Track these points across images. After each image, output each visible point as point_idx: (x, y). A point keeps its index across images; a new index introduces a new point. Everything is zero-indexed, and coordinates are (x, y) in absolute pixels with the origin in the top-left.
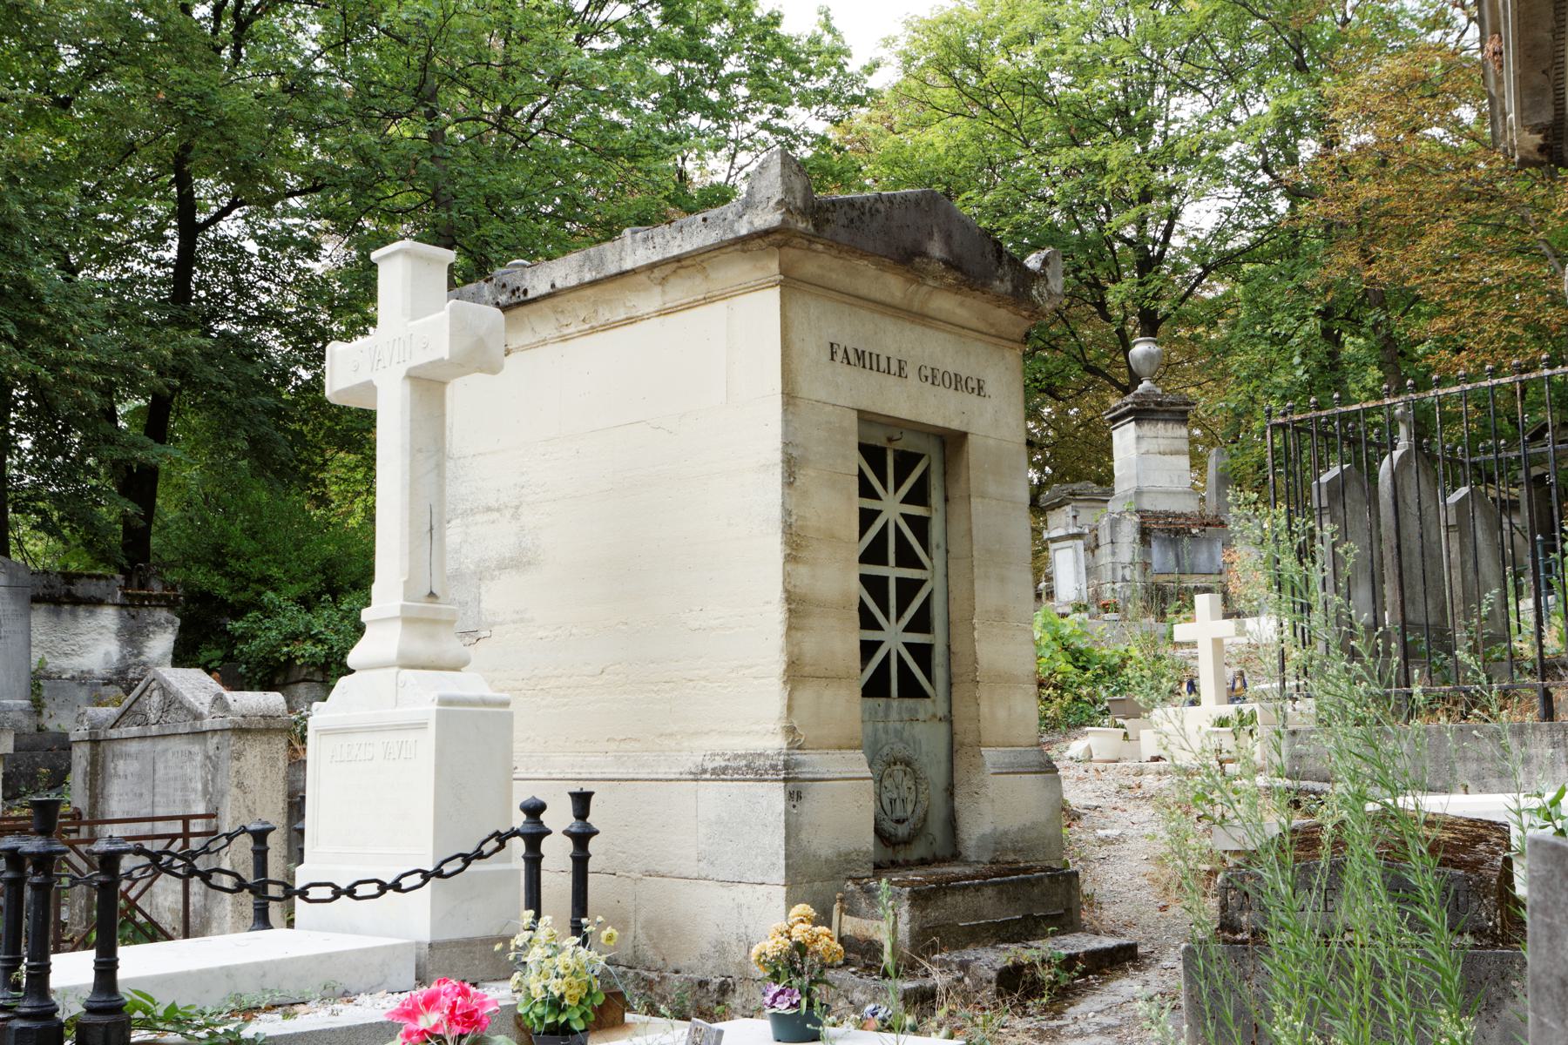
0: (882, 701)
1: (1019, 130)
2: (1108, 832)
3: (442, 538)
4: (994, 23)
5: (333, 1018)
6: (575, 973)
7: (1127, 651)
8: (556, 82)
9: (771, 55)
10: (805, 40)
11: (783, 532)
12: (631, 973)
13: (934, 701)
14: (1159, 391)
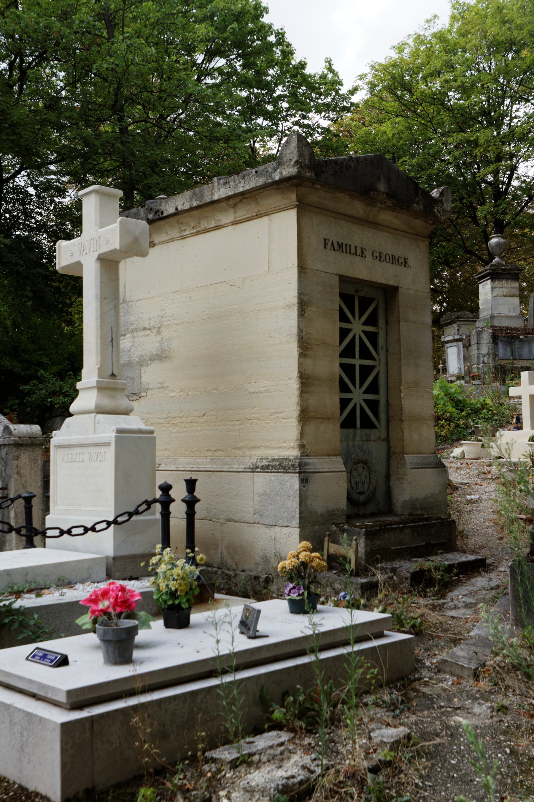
0: (351, 430)
1: (432, 124)
2: (473, 497)
3: (118, 345)
4: (419, 65)
5: (61, 597)
6: (183, 578)
7: (484, 401)
8: (186, 102)
9: (300, 85)
10: (318, 77)
11: (299, 341)
12: (220, 572)
13: (379, 430)
14: (504, 263)
